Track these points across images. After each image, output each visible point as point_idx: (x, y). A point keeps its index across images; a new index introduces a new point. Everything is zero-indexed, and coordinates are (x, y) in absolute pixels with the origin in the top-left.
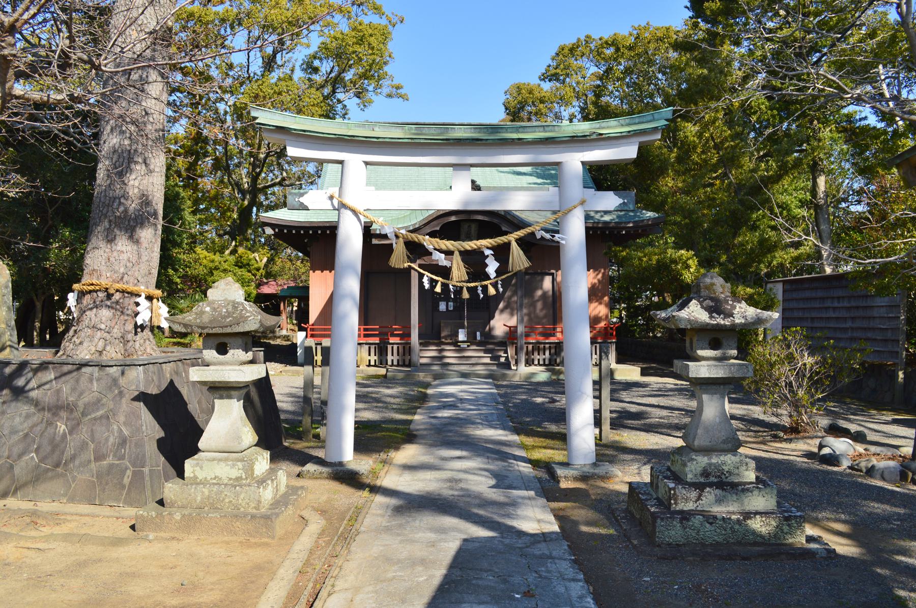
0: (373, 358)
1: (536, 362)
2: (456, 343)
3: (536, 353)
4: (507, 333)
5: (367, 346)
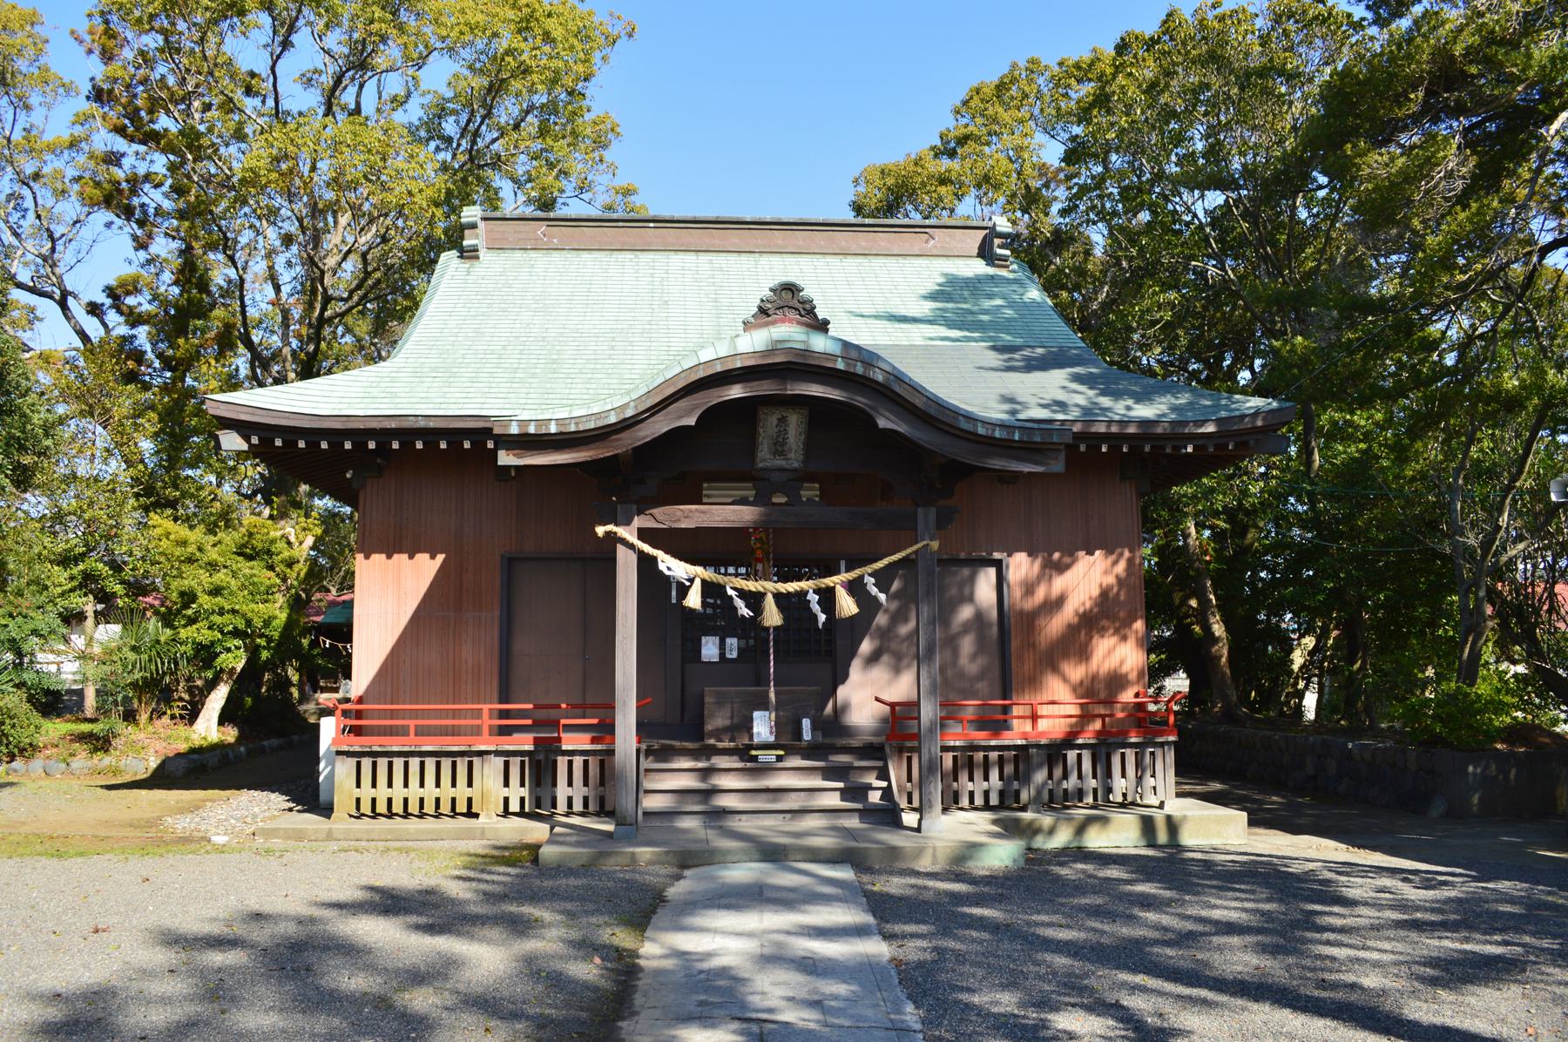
1: (965, 802)
2: (744, 753)
3: (963, 777)
4: (884, 720)
5: (500, 761)
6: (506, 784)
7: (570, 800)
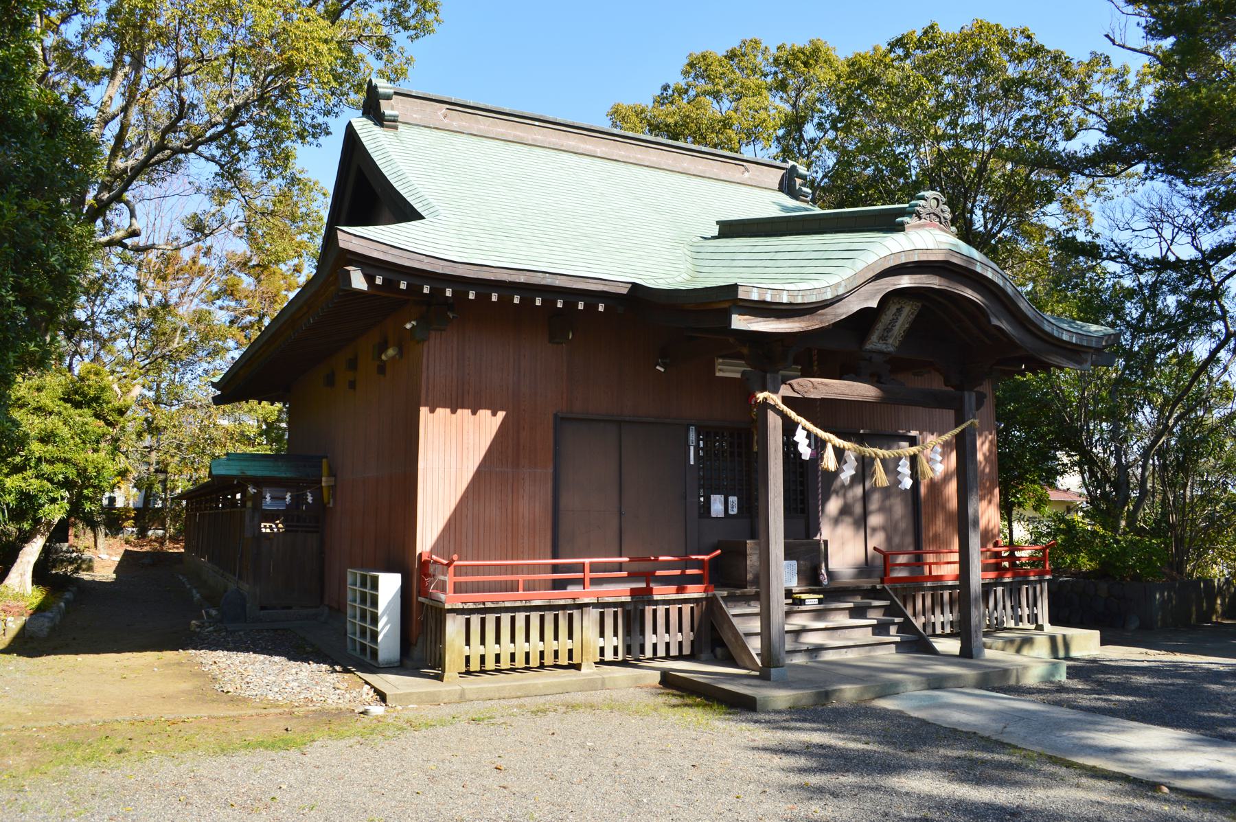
0: (612, 641)
6: (602, 634)
7: (655, 646)
